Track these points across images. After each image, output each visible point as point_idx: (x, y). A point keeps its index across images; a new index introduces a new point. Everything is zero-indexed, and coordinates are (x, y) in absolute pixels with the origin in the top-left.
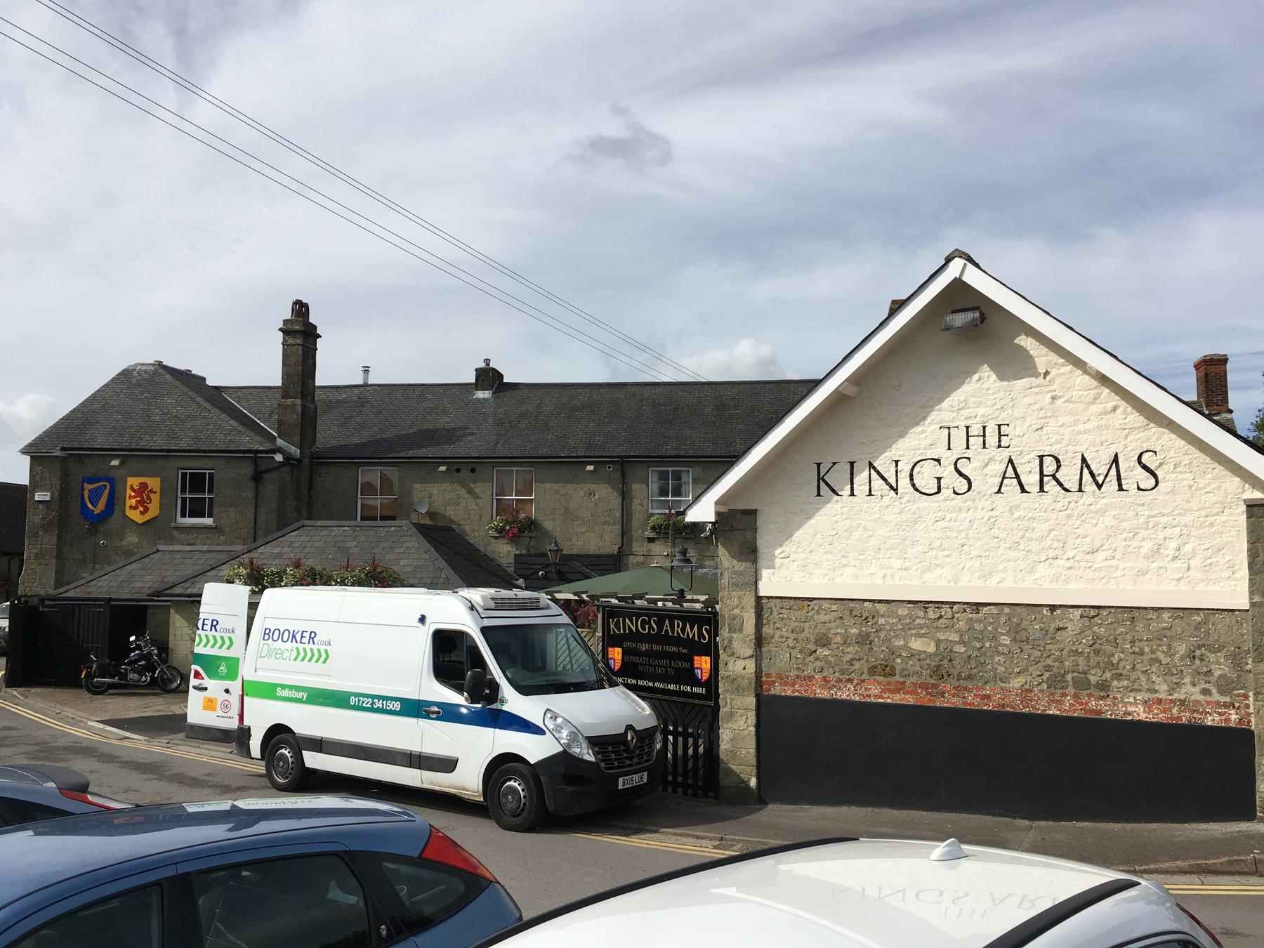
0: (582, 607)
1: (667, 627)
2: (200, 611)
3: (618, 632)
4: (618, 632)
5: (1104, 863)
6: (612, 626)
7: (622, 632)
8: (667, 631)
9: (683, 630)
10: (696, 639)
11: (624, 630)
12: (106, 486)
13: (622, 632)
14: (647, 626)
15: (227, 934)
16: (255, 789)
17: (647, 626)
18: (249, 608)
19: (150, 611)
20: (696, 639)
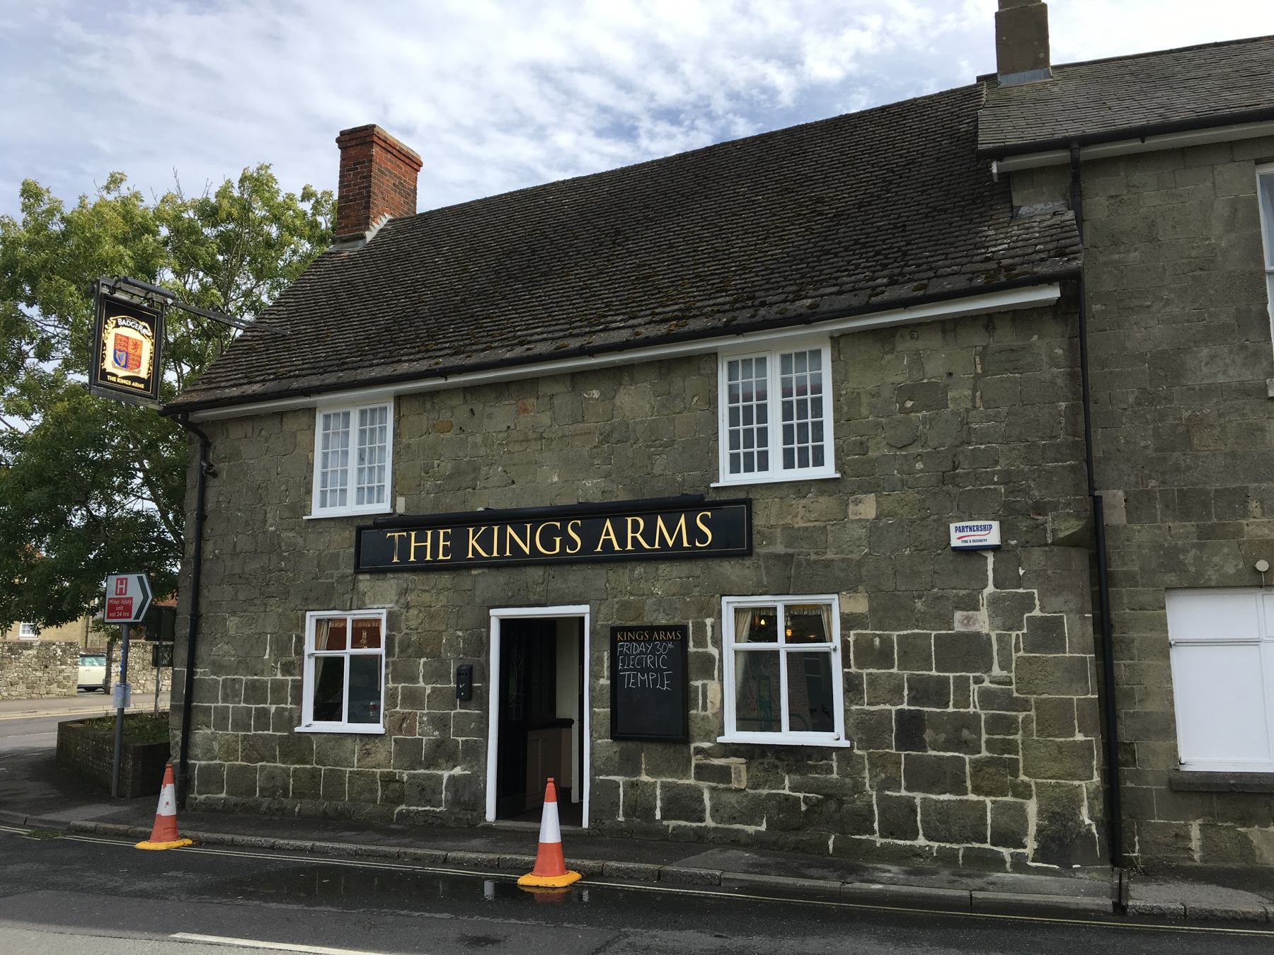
0: (180, 324)
1: (608, 534)
2: (1173, 635)
3: (646, 546)
4: (646, 546)
5: (336, 943)
6: (472, 542)
7: (495, 554)
8: (608, 543)
9: (649, 534)
10: (685, 544)
11: (502, 549)
12: (695, 748)
13: (495, 554)
14: (558, 540)
15: (668, 868)
16: (911, 444)
17: (558, 540)
18: (766, 392)
19: (754, 502)
20: (685, 544)
